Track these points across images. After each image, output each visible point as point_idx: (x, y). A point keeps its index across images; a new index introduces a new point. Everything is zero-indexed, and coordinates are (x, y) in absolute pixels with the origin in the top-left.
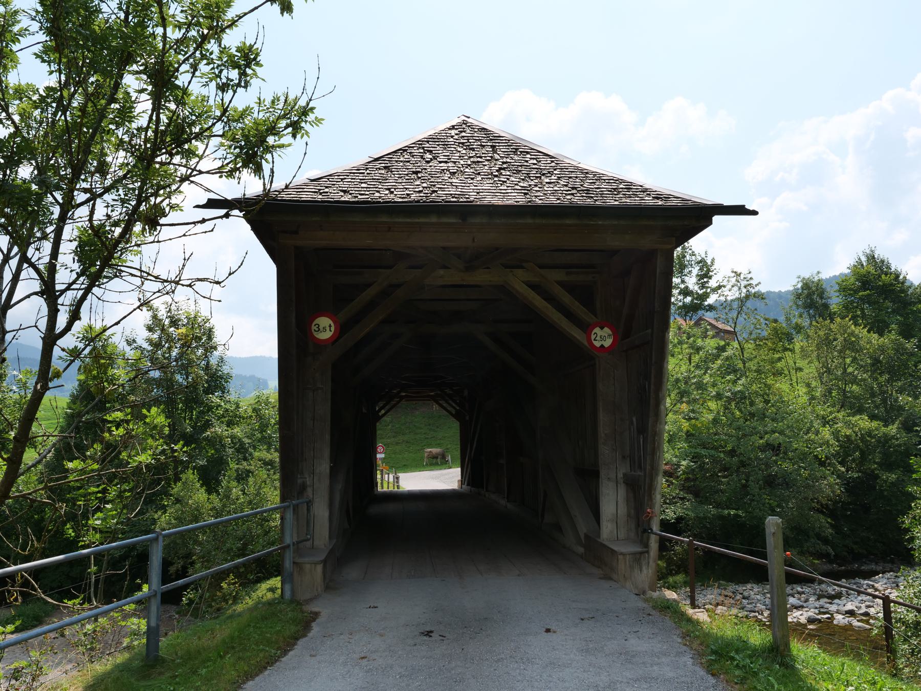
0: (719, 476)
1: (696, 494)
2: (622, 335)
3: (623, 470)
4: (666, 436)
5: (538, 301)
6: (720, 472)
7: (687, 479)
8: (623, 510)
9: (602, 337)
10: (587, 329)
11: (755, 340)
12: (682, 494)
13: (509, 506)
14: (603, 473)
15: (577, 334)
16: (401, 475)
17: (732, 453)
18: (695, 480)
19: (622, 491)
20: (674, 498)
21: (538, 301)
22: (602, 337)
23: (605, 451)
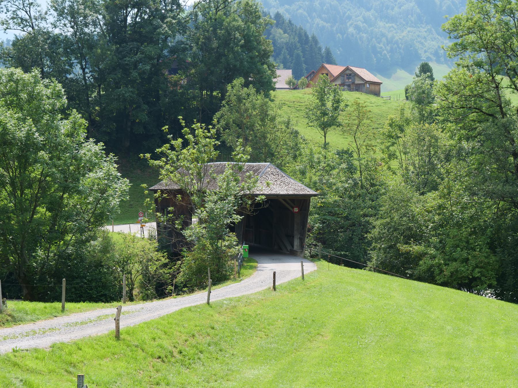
0: (338, 232)
1: (324, 243)
2: (300, 210)
3: (299, 236)
4: (307, 229)
5: (284, 202)
6: (339, 229)
7: (319, 233)
8: (299, 244)
9: (296, 210)
10: (293, 208)
11: (366, 146)
12: (314, 243)
13: (255, 245)
14: (295, 237)
15: (291, 209)
16: (115, 227)
17: (346, 218)
18: (323, 234)
19: (299, 239)
20: (310, 245)
21: (284, 202)
22: (296, 210)
23: (295, 232)
